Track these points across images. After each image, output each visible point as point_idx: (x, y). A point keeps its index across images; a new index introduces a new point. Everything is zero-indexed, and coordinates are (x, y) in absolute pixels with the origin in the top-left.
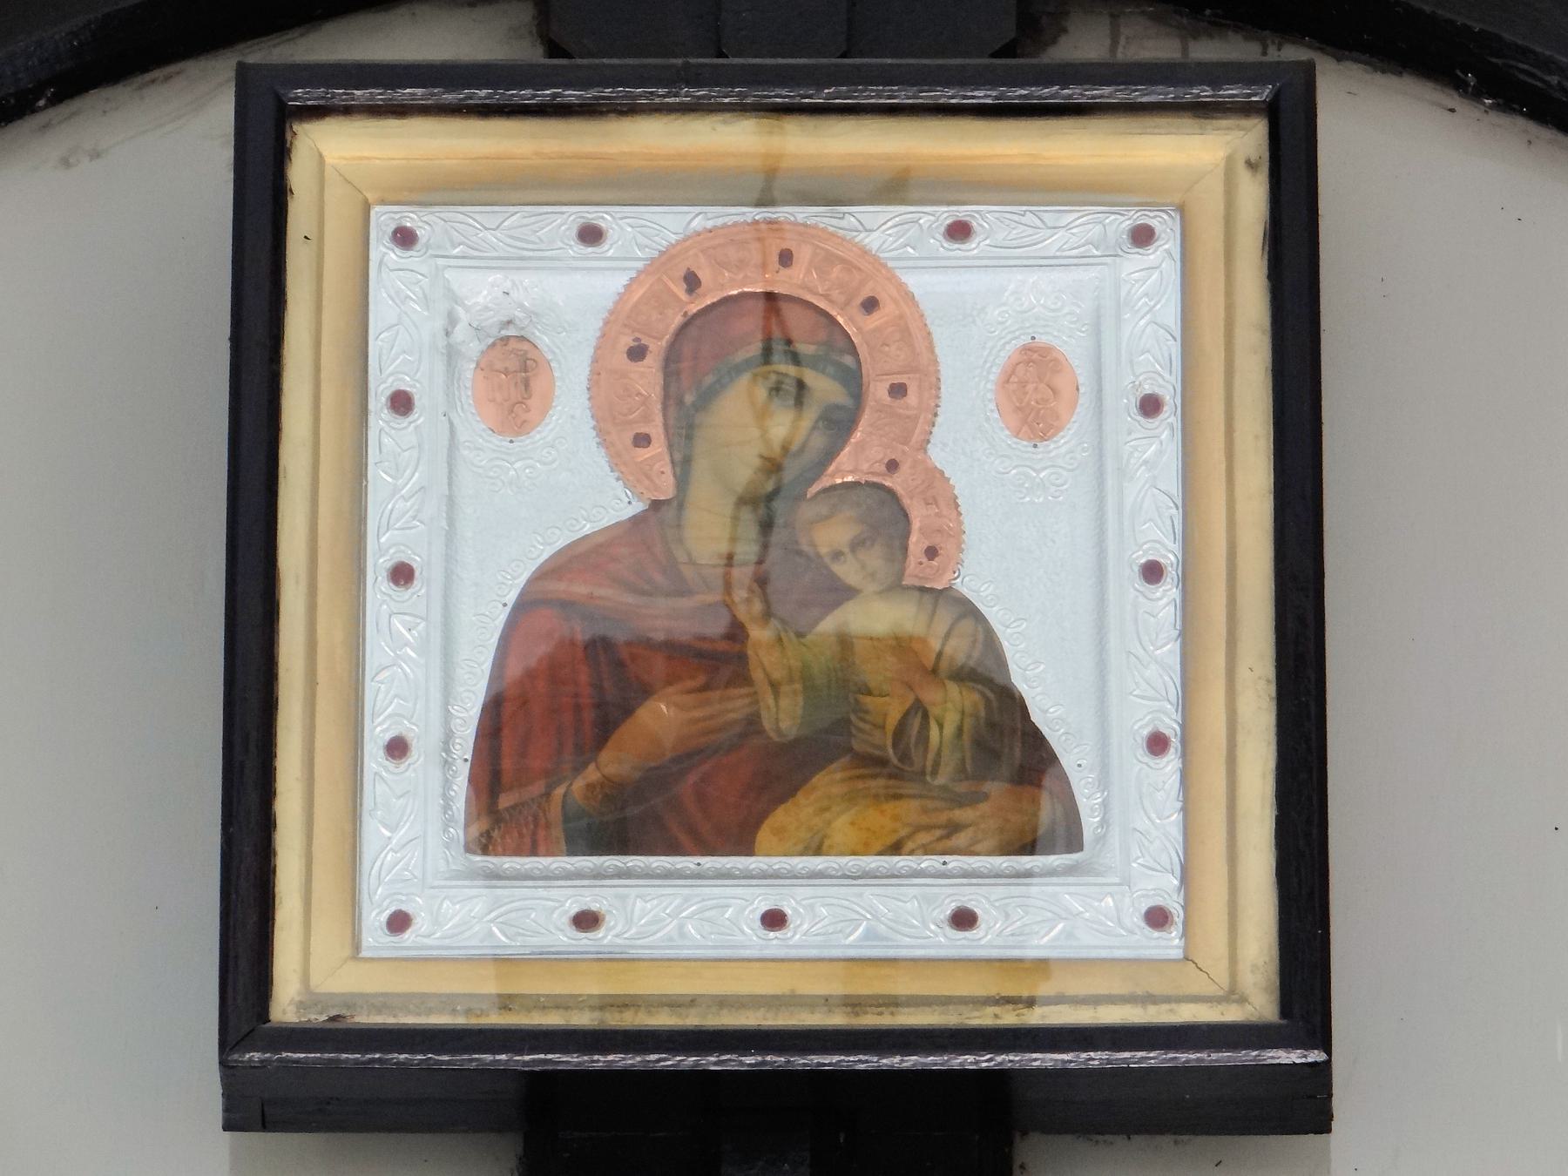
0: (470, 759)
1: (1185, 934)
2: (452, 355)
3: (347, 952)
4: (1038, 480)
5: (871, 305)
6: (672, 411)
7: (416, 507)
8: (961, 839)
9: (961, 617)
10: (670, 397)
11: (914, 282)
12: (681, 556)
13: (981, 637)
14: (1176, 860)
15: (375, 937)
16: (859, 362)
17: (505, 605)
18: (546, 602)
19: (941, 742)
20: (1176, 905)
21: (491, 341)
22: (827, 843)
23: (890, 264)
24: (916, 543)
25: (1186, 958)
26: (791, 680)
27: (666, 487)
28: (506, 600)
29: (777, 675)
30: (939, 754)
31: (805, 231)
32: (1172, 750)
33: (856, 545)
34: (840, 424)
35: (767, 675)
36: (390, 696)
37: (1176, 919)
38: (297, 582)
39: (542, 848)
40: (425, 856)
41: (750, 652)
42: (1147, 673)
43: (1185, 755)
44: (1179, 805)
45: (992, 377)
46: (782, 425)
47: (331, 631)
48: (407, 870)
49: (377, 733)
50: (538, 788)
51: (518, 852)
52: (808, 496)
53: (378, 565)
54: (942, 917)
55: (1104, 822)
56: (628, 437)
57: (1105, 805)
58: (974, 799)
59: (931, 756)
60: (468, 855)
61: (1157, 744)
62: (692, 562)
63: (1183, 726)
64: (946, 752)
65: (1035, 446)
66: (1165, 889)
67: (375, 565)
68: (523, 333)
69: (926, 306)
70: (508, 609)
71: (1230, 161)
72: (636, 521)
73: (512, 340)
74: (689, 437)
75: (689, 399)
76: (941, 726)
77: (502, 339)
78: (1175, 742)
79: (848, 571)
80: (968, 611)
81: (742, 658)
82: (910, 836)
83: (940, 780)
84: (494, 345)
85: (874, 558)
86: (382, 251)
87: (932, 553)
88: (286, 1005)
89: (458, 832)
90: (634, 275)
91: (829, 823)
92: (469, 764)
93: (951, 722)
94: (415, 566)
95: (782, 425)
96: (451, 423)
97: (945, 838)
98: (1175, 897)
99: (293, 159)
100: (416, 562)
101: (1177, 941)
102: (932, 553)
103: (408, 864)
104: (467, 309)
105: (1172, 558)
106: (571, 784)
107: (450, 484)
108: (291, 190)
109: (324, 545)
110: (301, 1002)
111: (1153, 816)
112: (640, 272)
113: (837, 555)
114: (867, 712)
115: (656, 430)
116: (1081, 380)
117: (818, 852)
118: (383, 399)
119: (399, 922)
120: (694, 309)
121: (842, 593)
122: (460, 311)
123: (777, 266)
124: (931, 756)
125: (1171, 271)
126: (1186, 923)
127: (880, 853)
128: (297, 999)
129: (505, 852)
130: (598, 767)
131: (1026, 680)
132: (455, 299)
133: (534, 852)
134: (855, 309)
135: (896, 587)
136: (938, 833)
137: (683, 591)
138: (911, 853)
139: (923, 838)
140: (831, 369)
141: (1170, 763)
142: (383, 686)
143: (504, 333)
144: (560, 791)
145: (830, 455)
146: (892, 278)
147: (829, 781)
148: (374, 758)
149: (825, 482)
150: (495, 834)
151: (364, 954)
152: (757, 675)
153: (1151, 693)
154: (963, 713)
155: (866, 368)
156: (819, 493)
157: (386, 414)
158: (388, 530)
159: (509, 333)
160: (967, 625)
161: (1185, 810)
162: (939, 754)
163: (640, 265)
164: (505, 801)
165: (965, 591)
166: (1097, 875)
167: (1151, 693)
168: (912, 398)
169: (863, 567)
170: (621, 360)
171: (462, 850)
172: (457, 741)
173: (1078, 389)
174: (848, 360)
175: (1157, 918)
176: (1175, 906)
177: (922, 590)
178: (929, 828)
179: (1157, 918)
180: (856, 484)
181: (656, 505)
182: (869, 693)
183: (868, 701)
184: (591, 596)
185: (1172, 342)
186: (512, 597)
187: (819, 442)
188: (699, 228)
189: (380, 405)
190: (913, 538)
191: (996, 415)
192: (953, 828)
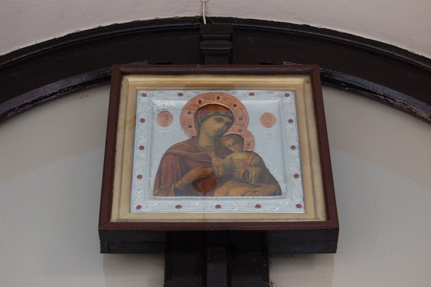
0: (155, 180)
1: (305, 209)
2: (153, 114)
3: (128, 212)
4: (269, 134)
5: (235, 106)
6: (196, 122)
7: (145, 137)
8: (257, 193)
9: (255, 156)
10: (196, 118)
11: (244, 102)
12: (198, 146)
13: (259, 159)
14: (302, 196)
15: (134, 210)
16: (233, 115)
17: (162, 154)
18: (171, 153)
19: (252, 176)
20: (302, 204)
21: (160, 112)
22: (229, 194)
23: (238, 99)
24: (245, 143)
25: (306, 213)
26: (221, 166)
27: (195, 134)
28: (163, 153)
29: (218, 166)
30: (251, 179)
31: (222, 94)
32: (299, 177)
33: (233, 144)
34: (229, 125)
35: (216, 165)
36: (139, 168)
37: (303, 206)
38: (120, 147)
39: (169, 195)
40: (145, 195)
41: (213, 162)
42: (293, 164)
43: (302, 178)
44: (302, 186)
45: (259, 118)
46: (219, 126)
47: (127, 155)
48: (141, 198)
49: (136, 173)
50: (168, 185)
51: (164, 196)
52: (224, 136)
53: (137, 146)
54: (254, 206)
55: (286, 190)
56: (187, 126)
57: (286, 187)
58: (259, 186)
59: (250, 179)
60: (154, 196)
61: (296, 176)
62: (200, 147)
63: (302, 173)
64: (253, 179)
65: (267, 112)
66: (300, 201)
67: (136, 147)
68: (167, 111)
69: (248, 108)
70: (163, 155)
71: (304, 82)
72: (189, 140)
73: (165, 112)
74: (200, 126)
75: (200, 121)
76: (252, 174)
77: (163, 112)
78: (300, 176)
79: (232, 148)
80: (256, 155)
81: (211, 163)
82: (246, 193)
83: (252, 183)
84: (161, 113)
85: (237, 146)
86: (140, 97)
87: (249, 145)
88: (114, 218)
89: (152, 192)
90: (189, 101)
91: (229, 191)
92: (154, 180)
93: (254, 174)
94: (144, 146)
95: (219, 126)
96: (152, 125)
97: (254, 193)
98: (302, 203)
99: (123, 81)
100: (144, 146)
101: (303, 210)
102: (249, 145)
103: (141, 197)
104: (156, 107)
105: (297, 145)
106: (175, 184)
107: (152, 134)
108: (122, 85)
109: (126, 142)
110: (117, 220)
111: (297, 189)
112: (190, 100)
113: (229, 146)
114: (236, 172)
115: (193, 125)
116: (276, 118)
117: (227, 196)
118: (139, 120)
119: (139, 207)
120: (200, 107)
121: (231, 152)
122: (155, 107)
123: (217, 99)
124: (250, 179)
125: (298, 151)
126: (305, 207)
127: (240, 196)
128: (116, 219)
129: (162, 196)
130: (181, 181)
131: (269, 166)
132: (153, 104)
133: (168, 196)
134: (232, 106)
135: (242, 151)
136: (252, 192)
137: (199, 151)
138: (247, 196)
139: (249, 193)
140: (228, 116)
141: (300, 179)
142: (137, 166)
143: (163, 110)
144: (173, 186)
145: (228, 129)
146: (239, 102)
147: (229, 183)
148: (135, 179)
149: (227, 133)
150: (159, 193)
151: (131, 212)
152: (214, 165)
153: (294, 167)
154: (256, 172)
155: (234, 116)
156: (226, 136)
157: (140, 122)
158: (139, 140)
159: (164, 111)
160: (256, 157)
161: (303, 187)
162: (251, 179)
163: (190, 99)
164: (162, 187)
165: (256, 152)
166: (286, 198)
167: (294, 167)
168: (244, 120)
169: (235, 148)
170: (186, 114)
171: (153, 195)
172: (152, 176)
173: (276, 120)
174: (231, 115)
175: (299, 206)
176: (302, 204)
177: (247, 151)
178: (250, 191)
179: (299, 206)
180: (233, 134)
181: (193, 137)
182: (237, 168)
183: (237, 170)
184: (161, 26)
185: (294, 111)
186: (164, 153)
187: (225, 128)
188: (201, 94)
189: (138, 121)
190: (245, 142)
191: (260, 123)
192: (255, 192)
